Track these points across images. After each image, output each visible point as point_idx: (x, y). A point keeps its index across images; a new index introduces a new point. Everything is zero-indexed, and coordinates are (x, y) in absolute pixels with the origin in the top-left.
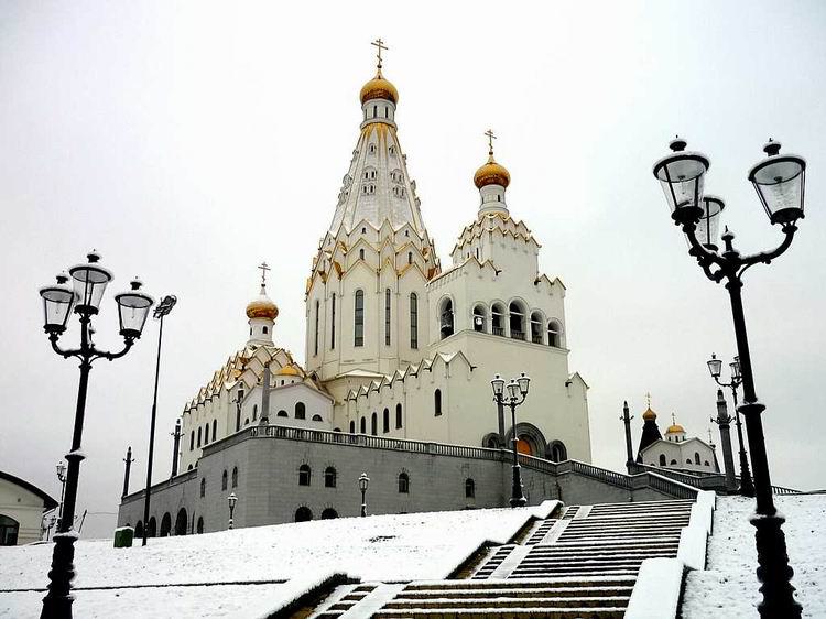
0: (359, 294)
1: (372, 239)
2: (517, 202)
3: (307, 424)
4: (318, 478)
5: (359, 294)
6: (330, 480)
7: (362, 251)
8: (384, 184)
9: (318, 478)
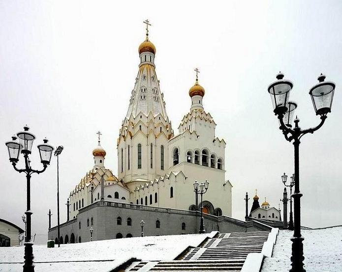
0: (140, 146)
1: (144, 120)
2: (208, 104)
3: (119, 201)
4: (124, 222)
5: (140, 146)
6: (129, 222)
7: (140, 126)
8: (150, 94)
9: (124, 222)
